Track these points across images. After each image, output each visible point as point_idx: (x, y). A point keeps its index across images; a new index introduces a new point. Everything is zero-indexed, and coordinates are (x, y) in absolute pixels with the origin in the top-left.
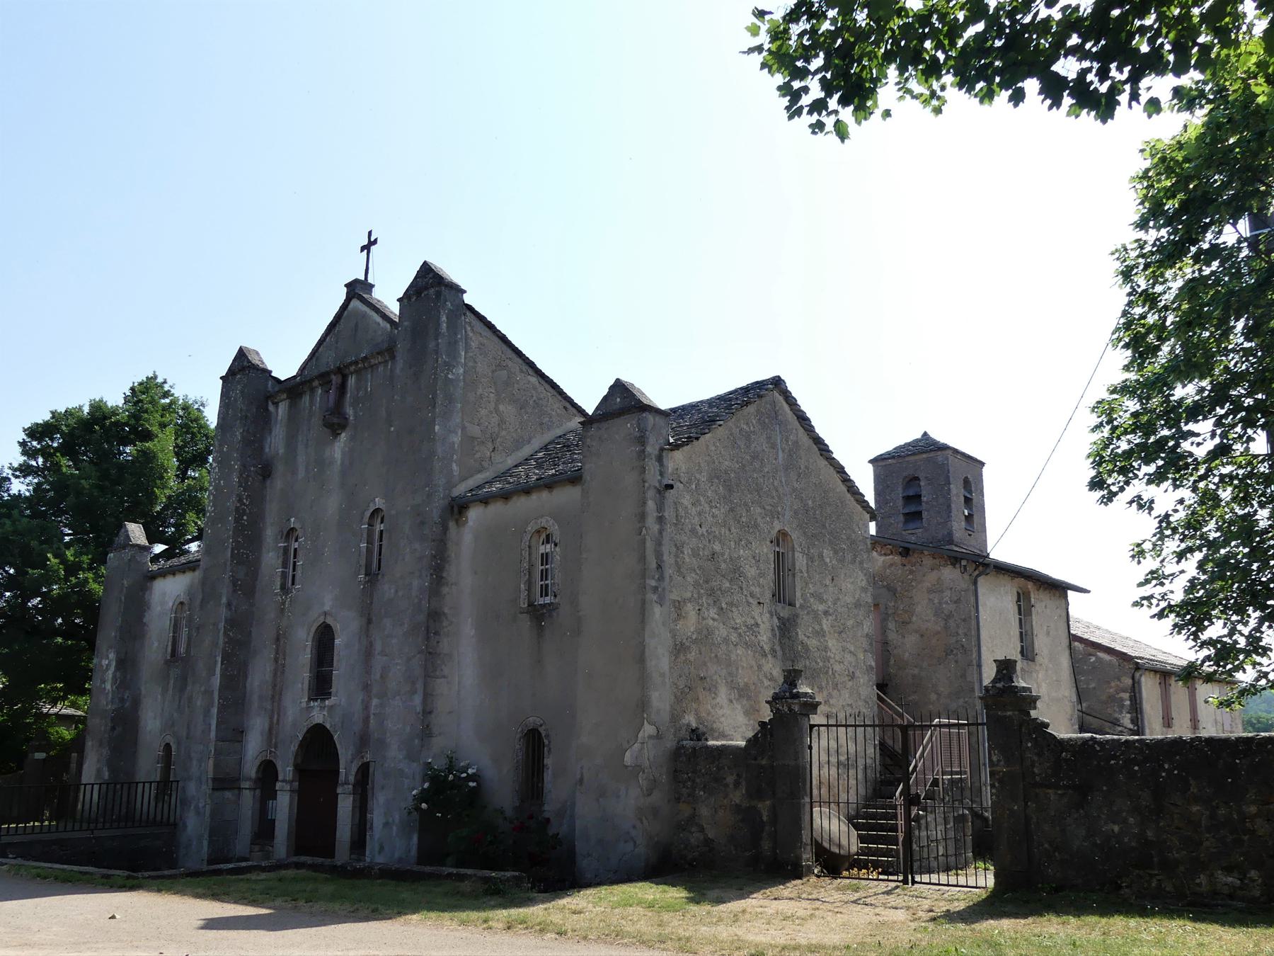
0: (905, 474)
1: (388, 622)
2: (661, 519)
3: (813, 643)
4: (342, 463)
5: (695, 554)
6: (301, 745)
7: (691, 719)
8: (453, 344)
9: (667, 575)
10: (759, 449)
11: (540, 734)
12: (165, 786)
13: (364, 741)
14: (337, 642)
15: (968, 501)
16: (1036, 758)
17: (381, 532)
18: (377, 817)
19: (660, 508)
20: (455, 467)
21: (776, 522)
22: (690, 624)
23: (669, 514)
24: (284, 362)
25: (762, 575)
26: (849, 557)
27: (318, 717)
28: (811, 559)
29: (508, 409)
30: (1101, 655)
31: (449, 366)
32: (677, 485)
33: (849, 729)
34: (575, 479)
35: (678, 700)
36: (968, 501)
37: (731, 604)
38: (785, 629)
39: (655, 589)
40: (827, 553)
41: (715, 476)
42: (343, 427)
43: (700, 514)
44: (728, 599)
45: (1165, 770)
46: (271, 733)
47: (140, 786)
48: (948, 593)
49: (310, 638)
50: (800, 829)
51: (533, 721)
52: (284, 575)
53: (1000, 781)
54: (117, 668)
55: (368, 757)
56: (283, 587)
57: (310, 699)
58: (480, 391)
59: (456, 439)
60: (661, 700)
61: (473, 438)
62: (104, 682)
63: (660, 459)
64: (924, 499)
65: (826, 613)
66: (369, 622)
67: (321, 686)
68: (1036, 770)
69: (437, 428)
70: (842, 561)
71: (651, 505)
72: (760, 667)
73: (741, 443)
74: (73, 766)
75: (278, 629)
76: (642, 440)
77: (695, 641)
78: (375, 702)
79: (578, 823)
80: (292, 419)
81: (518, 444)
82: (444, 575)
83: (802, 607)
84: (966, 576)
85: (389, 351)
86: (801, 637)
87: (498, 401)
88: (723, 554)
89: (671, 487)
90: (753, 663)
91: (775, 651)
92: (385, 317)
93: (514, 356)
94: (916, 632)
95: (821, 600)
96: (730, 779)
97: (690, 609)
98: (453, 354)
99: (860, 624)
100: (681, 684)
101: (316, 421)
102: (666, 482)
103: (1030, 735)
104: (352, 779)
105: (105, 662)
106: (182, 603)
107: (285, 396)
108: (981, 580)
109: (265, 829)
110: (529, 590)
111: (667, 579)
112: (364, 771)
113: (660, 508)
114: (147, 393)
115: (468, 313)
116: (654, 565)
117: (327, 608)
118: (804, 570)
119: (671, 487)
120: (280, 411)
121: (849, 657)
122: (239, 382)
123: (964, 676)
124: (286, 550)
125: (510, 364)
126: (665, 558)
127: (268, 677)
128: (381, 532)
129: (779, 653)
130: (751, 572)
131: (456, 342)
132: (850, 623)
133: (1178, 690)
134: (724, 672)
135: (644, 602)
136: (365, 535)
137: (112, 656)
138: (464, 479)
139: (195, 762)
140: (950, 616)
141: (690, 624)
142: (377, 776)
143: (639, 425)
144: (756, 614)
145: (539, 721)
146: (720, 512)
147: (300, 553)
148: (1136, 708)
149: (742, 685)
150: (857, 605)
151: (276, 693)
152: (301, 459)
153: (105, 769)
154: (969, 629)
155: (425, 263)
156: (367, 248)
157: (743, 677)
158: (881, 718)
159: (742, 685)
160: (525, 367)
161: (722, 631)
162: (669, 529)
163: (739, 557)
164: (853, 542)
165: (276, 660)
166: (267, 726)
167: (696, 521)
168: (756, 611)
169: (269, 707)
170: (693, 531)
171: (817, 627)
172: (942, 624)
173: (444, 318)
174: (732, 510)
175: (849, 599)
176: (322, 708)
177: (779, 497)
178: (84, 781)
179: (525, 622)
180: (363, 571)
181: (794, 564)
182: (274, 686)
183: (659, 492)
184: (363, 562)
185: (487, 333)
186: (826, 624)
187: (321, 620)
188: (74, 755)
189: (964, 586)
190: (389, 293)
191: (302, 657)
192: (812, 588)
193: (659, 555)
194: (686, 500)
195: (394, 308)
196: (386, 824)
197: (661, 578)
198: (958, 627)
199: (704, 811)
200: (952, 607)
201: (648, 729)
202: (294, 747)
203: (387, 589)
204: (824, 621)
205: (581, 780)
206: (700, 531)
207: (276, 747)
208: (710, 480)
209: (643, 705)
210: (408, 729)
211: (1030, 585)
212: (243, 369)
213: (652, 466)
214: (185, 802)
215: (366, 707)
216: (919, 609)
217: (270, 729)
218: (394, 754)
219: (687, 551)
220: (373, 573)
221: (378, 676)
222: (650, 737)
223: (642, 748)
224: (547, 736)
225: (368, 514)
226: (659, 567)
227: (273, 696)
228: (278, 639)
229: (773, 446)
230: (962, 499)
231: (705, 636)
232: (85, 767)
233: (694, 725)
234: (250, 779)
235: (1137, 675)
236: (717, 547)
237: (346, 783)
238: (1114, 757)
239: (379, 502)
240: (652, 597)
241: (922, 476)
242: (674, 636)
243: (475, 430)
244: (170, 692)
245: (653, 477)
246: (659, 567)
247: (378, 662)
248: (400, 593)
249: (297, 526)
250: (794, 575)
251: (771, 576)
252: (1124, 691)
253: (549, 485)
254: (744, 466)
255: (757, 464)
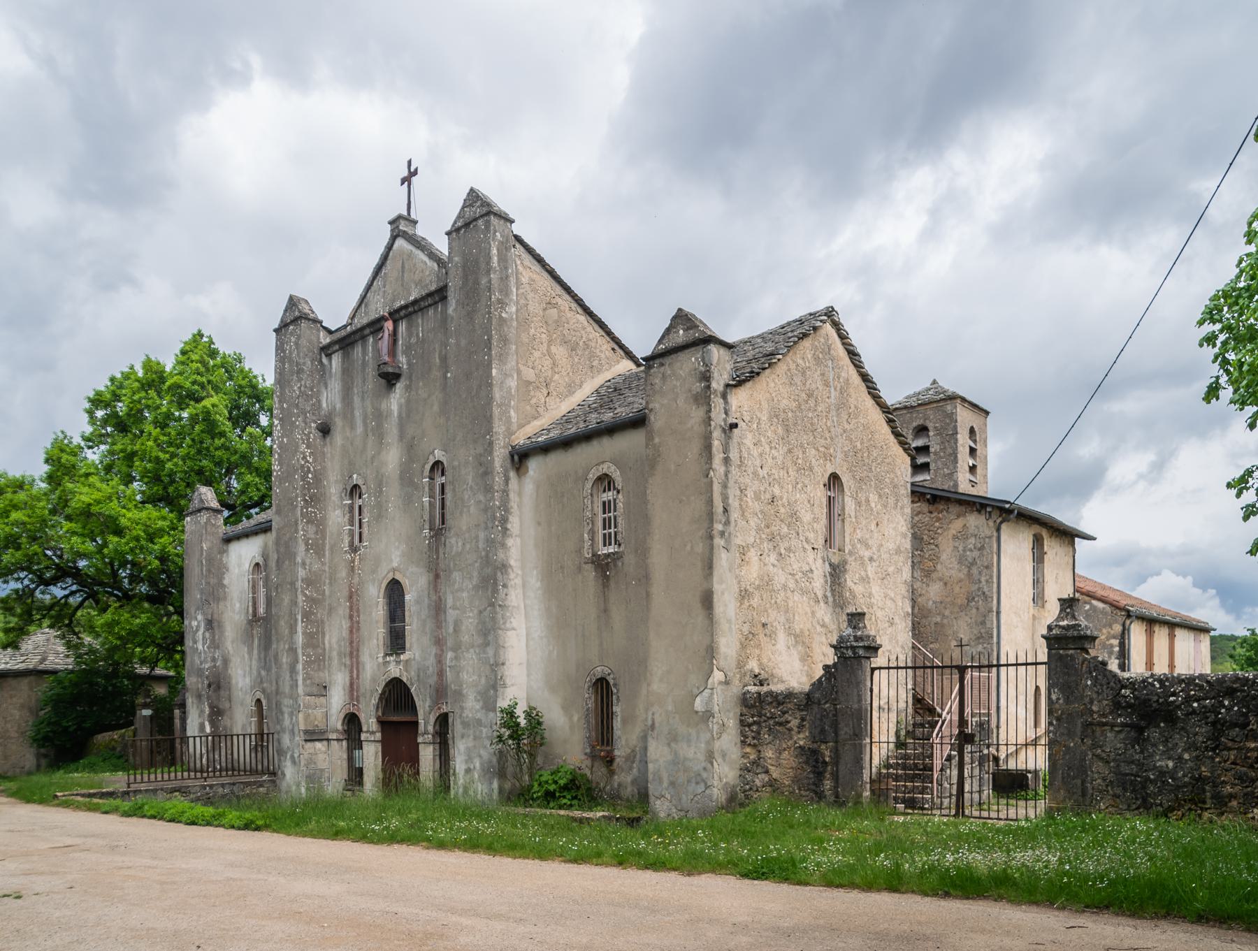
0: (915, 424)
1: (456, 575)
2: (727, 461)
3: (859, 589)
4: (400, 416)
5: (757, 497)
6: (380, 699)
7: (753, 665)
8: (505, 279)
9: (732, 519)
10: (814, 386)
11: (608, 683)
12: (262, 739)
13: (440, 692)
14: (407, 597)
15: (973, 451)
16: (1095, 696)
17: (443, 485)
18: (459, 764)
19: (726, 450)
20: (512, 413)
21: (829, 464)
22: (752, 572)
23: (734, 455)
24: (335, 312)
25: (816, 520)
26: (891, 501)
27: (395, 671)
28: (859, 504)
29: (560, 351)
30: (1094, 602)
31: (502, 304)
32: (741, 424)
33: (894, 665)
34: (638, 422)
35: (743, 647)
36: (973, 451)
37: (789, 550)
38: (836, 573)
39: (722, 534)
40: (873, 498)
41: (775, 415)
42: (397, 376)
43: (761, 455)
44: (786, 545)
45: (1224, 706)
46: (353, 689)
47: (235, 738)
48: (972, 540)
49: (382, 595)
50: (862, 768)
51: (599, 671)
52: (351, 533)
53: (1058, 719)
54: (207, 629)
55: (445, 709)
56: (351, 544)
57: (386, 655)
58: (532, 331)
59: (512, 383)
60: (728, 646)
61: (530, 383)
62: (195, 642)
63: (724, 396)
64: (932, 450)
65: (871, 559)
66: (437, 576)
67: (396, 642)
68: (1095, 708)
69: (494, 372)
70: (885, 506)
71: (716, 444)
72: (813, 613)
73: (798, 380)
74: (177, 722)
75: (350, 587)
76: (706, 377)
77: (758, 588)
78: (450, 655)
79: (651, 766)
80: (347, 372)
81: (571, 389)
82: (509, 526)
83: (851, 553)
84: (991, 523)
85: (440, 295)
86: (849, 583)
87: (550, 342)
88: (781, 498)
89: (736, 426)
90: (808, 610)
91: (826, 597)
92: (433, 255)
93: (563, 292)
94: (941, 579)
95: (867, 547)
96: (794, 723)
97: (752, 554)
98: (505, 291)
99: (899, 570)
100: (746, 629)
101: (371, 372)
102: (731, 420)
103: (1091, 673)
104: (431, 729)
105: (194, 623)
106: (257, 564)
107: (337, 347)
108: (1004, 526)
109: (356, 776)
110: (592, 539)
111: (733, 524)
112: (443, 721)
113: (726, 450)
114: (199, 349)
115: (518, 245)
116: (721, 510)
117: (395, 565)
118: (853, 514)
119: (736, 426)
120: (334, 362)
121: (889, 603)
122: (292, 334)
123: (983, 623)
124: (351, 507)
125: (560, 301)
126: (730, 501)
127: (345, 633)
128: (443, 485)
129: (831, 599)
130: (806, 517)
131: (507, 277)
132: (891, 569)
133: (1161, 635)
134: (782, 619)
135: (712, 547)
136: (427, 489)
137: (200, 617)
138: (521, 426)
139: (286, 716)
140: (973, 563)
141: (752, 572)
142: (456, 728)
143: (703, 360)
144: (811, 560)
145: (607, 671)
146: (780, 453)
147: (365, 510)
148: (1124, 655)
149: (798, 631)
150: (898, 551)
151: (353, 652)
152: (358, 413)
153: (207, 723)
154: (991, 577)
155: (472, 190)
156: (407, 180)
157: (800, 624)
158: (914, 661)
159: (798, 631)
160: (574, 305)
161: (780, 578)
162: (734, 470)
163: (796, 501)
164: (895, 487)
165: (351, 617)
166: (347, 679)
167: (758, 463)
168: (811, 555)
169: (348, 662)
170: (755, 474)
171: (863, 573)
172: (966, 571)
173: (495, 251)
174: (790, 451)
175: (891, 546)
176: (398, 663)
177: (832, 438)
178: (189, 733)
179: (590, 573)
180: (427, 526)
181: (843, 509)
182: (351, 643)
183: (724, 431)
184: (426, 517)
185: (537, 267)
186: (871, 569)
187: (390, 577)
188: (177, 712)
189: (988, 533)
190: (435, 229)
191: (377, 612)
192: (859, 534)
193: (725, 498)
194: (749, 441)
195: (442, 246)
196: (468, 771)
197: (727, 523)
198: (980, 573)
199: (769, 753)
200: (976, 553)
201: (718, 676)
202: (374, 701)
203: (454, 543)
204: (869, 568)
205: (653, 727)
206: (762, 473)
207: (358, 701)
208: (770, 419)
209: (711, 652)
210: (483, 680)
211: (1044, 533)
212: (295, 321)
213: (717, 402)
214: (281, 752)
215: (440, 660)
216: (944, 557)
217: (352, 684)
218: (472, 705)
219: (750, 493)
220: (439, 528)
221: (451, 630)
222: (721, 683)
223: (712, 694)
224: (615, 685)
225: (428, 467)
226: (726, 510)
227: (351, 653)
228: (351, 597)
229: (827, 384)
230: (968, 450)
231: (766, 583)
232: (189, 721)
233: (757, 671)
234: (337, 731)
235: (1128, 622)
236: (777, 491)
237: (426, 733)
238: (1174, 694)
239: (439, 455)
240: (718, 541)
241: (930, 425)
242: (739, 582)
243: (529, 374)
244: (255, 652)
245: (718, 417)
246: (726, 510)
247: (451, 614)
248: (468, 546)
249: (360, 483)
250: (843, 521)
251: (824, 521)
252: (1114, 637)
253: (611, 430)
254: (800, 405)
255: (812, 403)
